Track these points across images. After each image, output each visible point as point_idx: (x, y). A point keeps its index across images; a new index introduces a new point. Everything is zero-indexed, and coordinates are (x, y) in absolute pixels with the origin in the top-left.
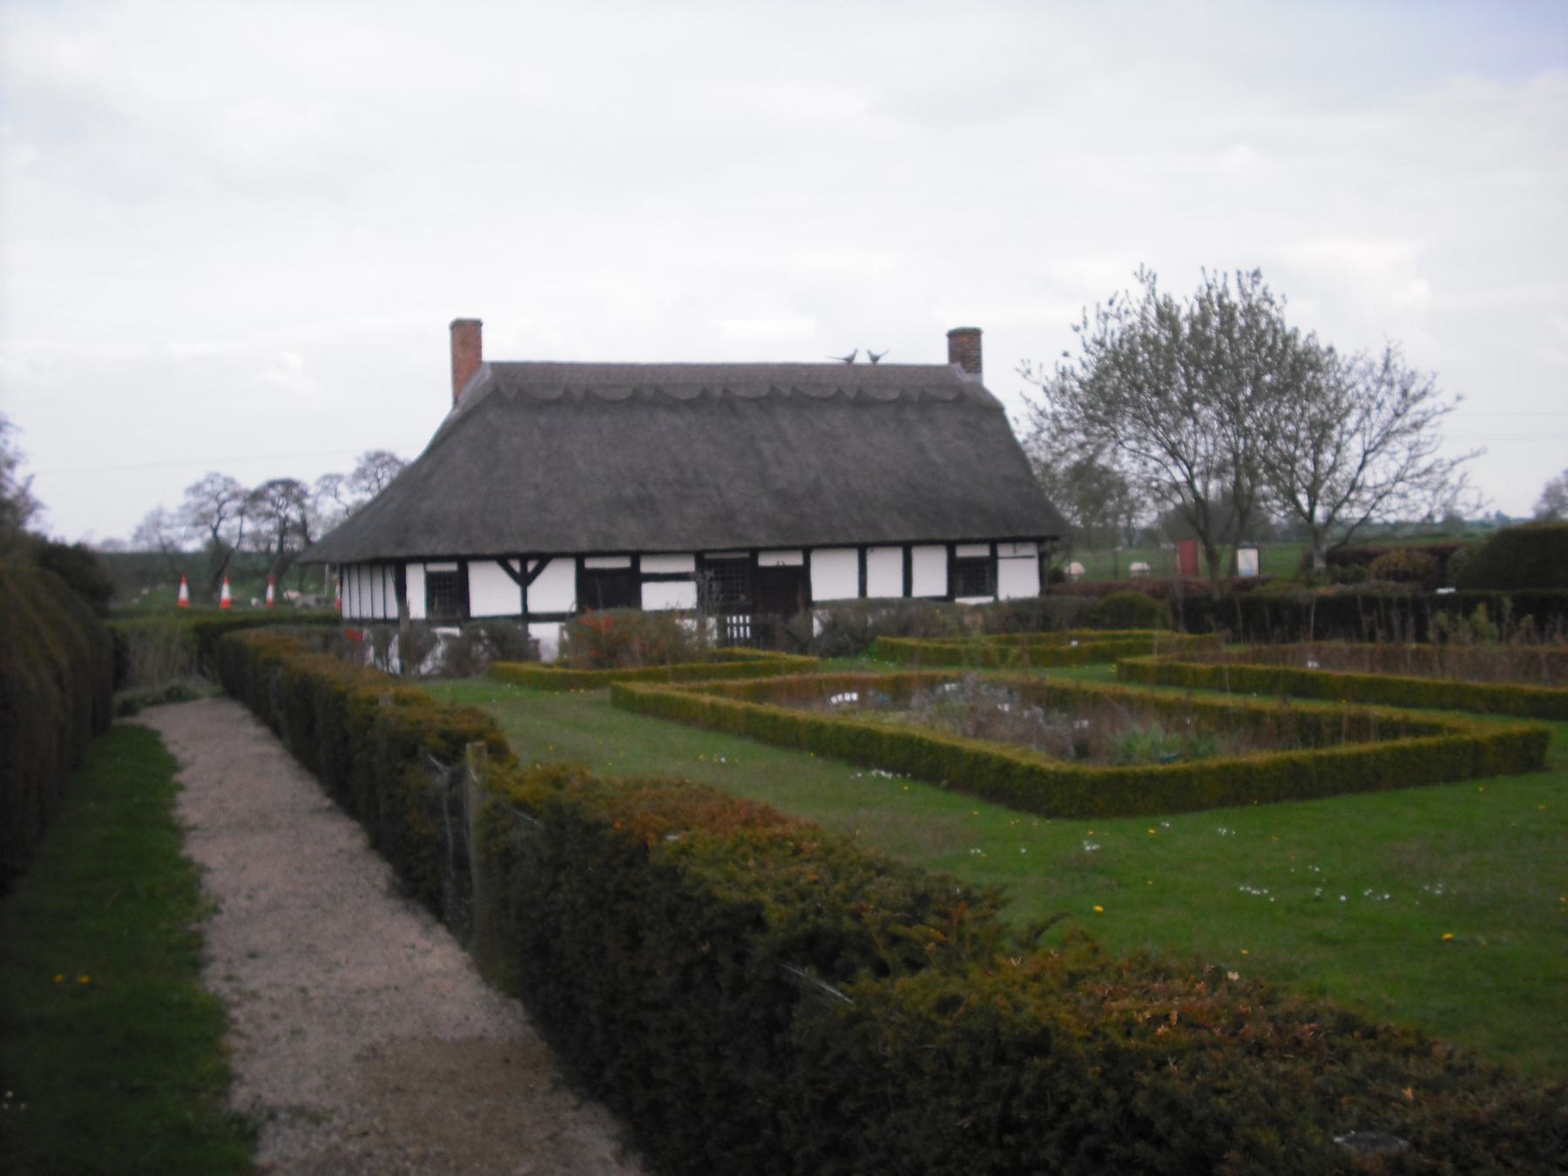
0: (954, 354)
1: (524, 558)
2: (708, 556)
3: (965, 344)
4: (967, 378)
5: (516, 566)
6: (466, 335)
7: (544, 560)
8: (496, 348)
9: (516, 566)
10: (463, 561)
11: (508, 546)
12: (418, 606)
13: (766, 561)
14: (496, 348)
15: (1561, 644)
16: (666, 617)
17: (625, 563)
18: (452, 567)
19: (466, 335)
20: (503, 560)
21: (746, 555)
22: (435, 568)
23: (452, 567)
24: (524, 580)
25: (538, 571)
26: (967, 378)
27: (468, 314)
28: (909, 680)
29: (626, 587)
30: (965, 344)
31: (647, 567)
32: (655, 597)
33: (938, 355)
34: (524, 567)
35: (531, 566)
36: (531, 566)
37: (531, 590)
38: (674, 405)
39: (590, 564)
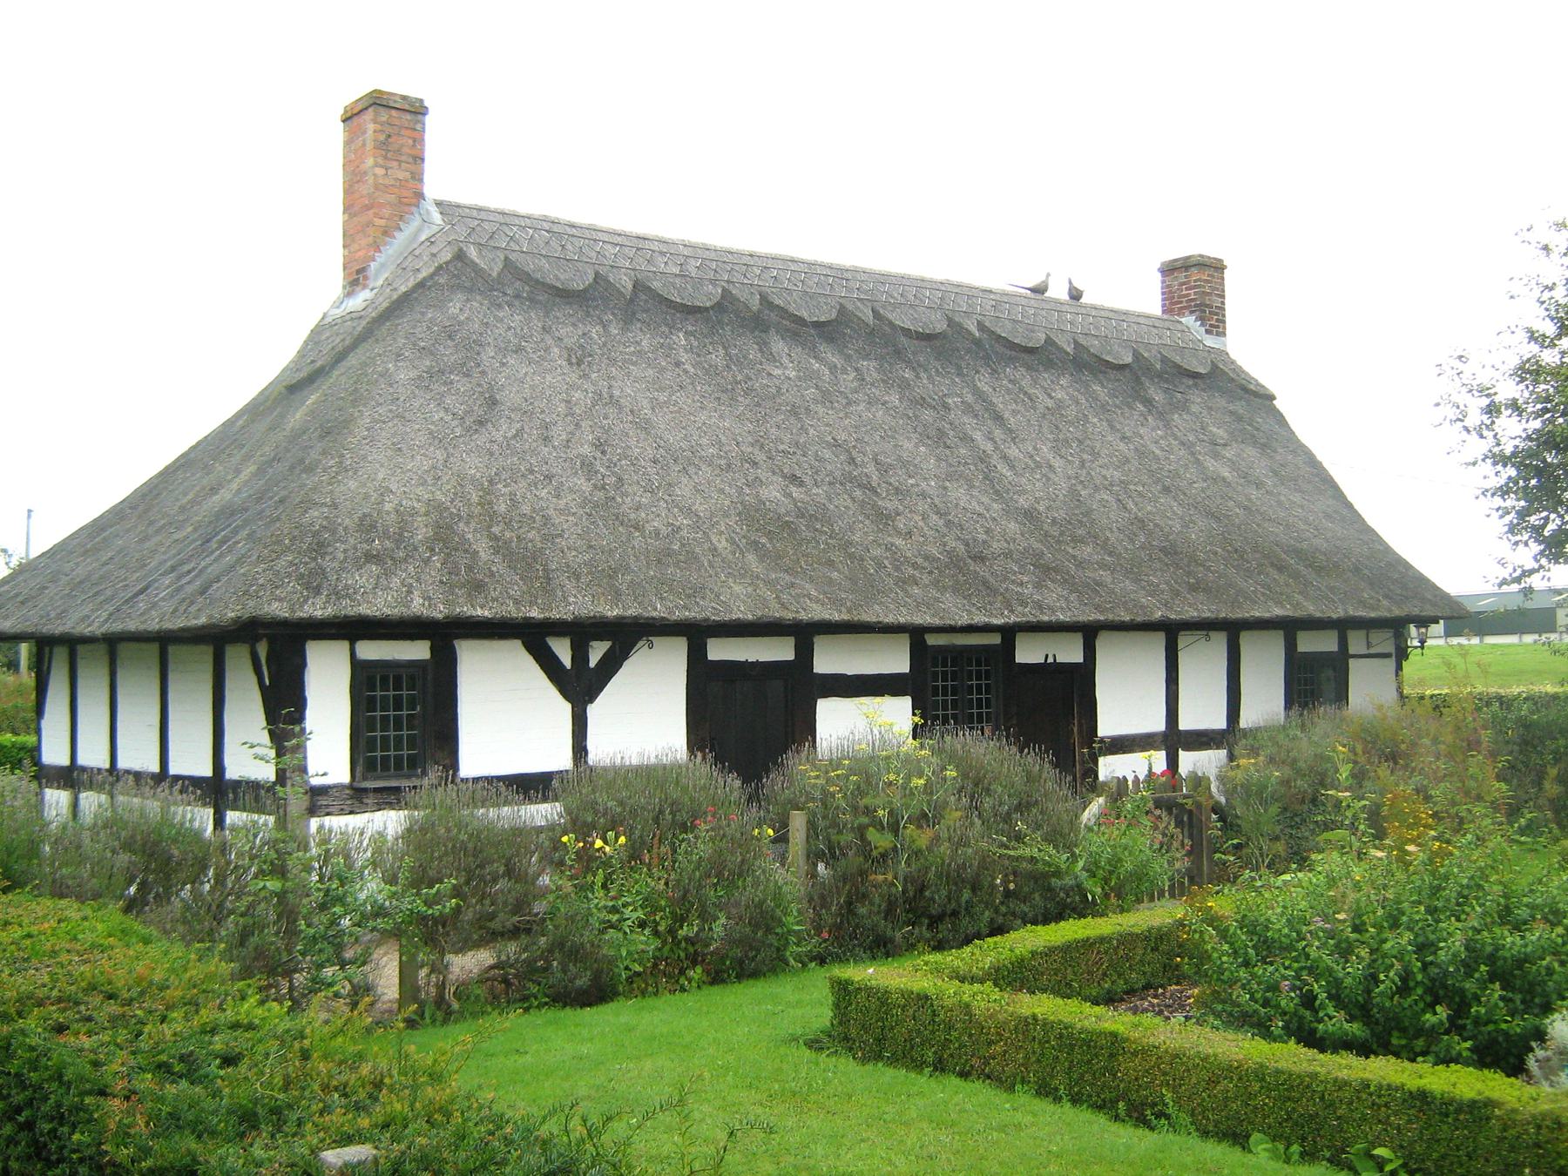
0: (1172, 303)
1: (581, 631)
2: (932, 640)
3: (1195, 284)
4: (1210, 341)
5: (562, 650)
6: (387, 128)
7: (626, 636)
8: (463, 169)
9: (562, 650)
10: (446, 635)
11: (577, 604)
12: (328, 750)
13: (1029, 653)
14: (463, 169)
15: (8, 738)
16: (864, 770)
17: (780, 651)
18: (418, 651)
19: (387, 128)
20: (534, 636)
21: (995, 639)
22: (371, 651)
23: (418, 651)
24: (580, 687)
25: (611, 666)
26: (1210, 341)
27: (398, 84)
28: (1186, 885)
29: (790, 696)
30: (1195, 284)
31: (829, 660)
32: (839, 724)
33: (1146, 298)
34: (580, 654)
35: (597, 652)
36: (597, 652)
37: (593, 710)
38: (801, 330)
39: (719, 650)
